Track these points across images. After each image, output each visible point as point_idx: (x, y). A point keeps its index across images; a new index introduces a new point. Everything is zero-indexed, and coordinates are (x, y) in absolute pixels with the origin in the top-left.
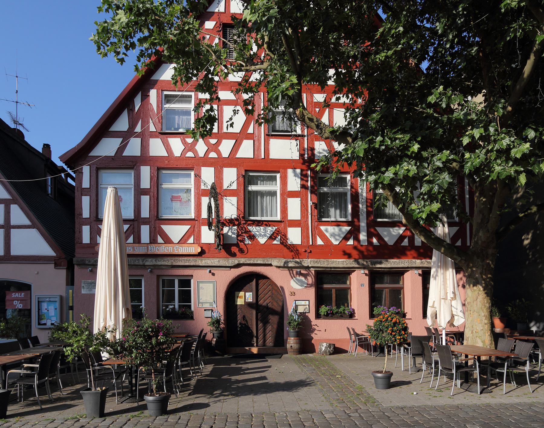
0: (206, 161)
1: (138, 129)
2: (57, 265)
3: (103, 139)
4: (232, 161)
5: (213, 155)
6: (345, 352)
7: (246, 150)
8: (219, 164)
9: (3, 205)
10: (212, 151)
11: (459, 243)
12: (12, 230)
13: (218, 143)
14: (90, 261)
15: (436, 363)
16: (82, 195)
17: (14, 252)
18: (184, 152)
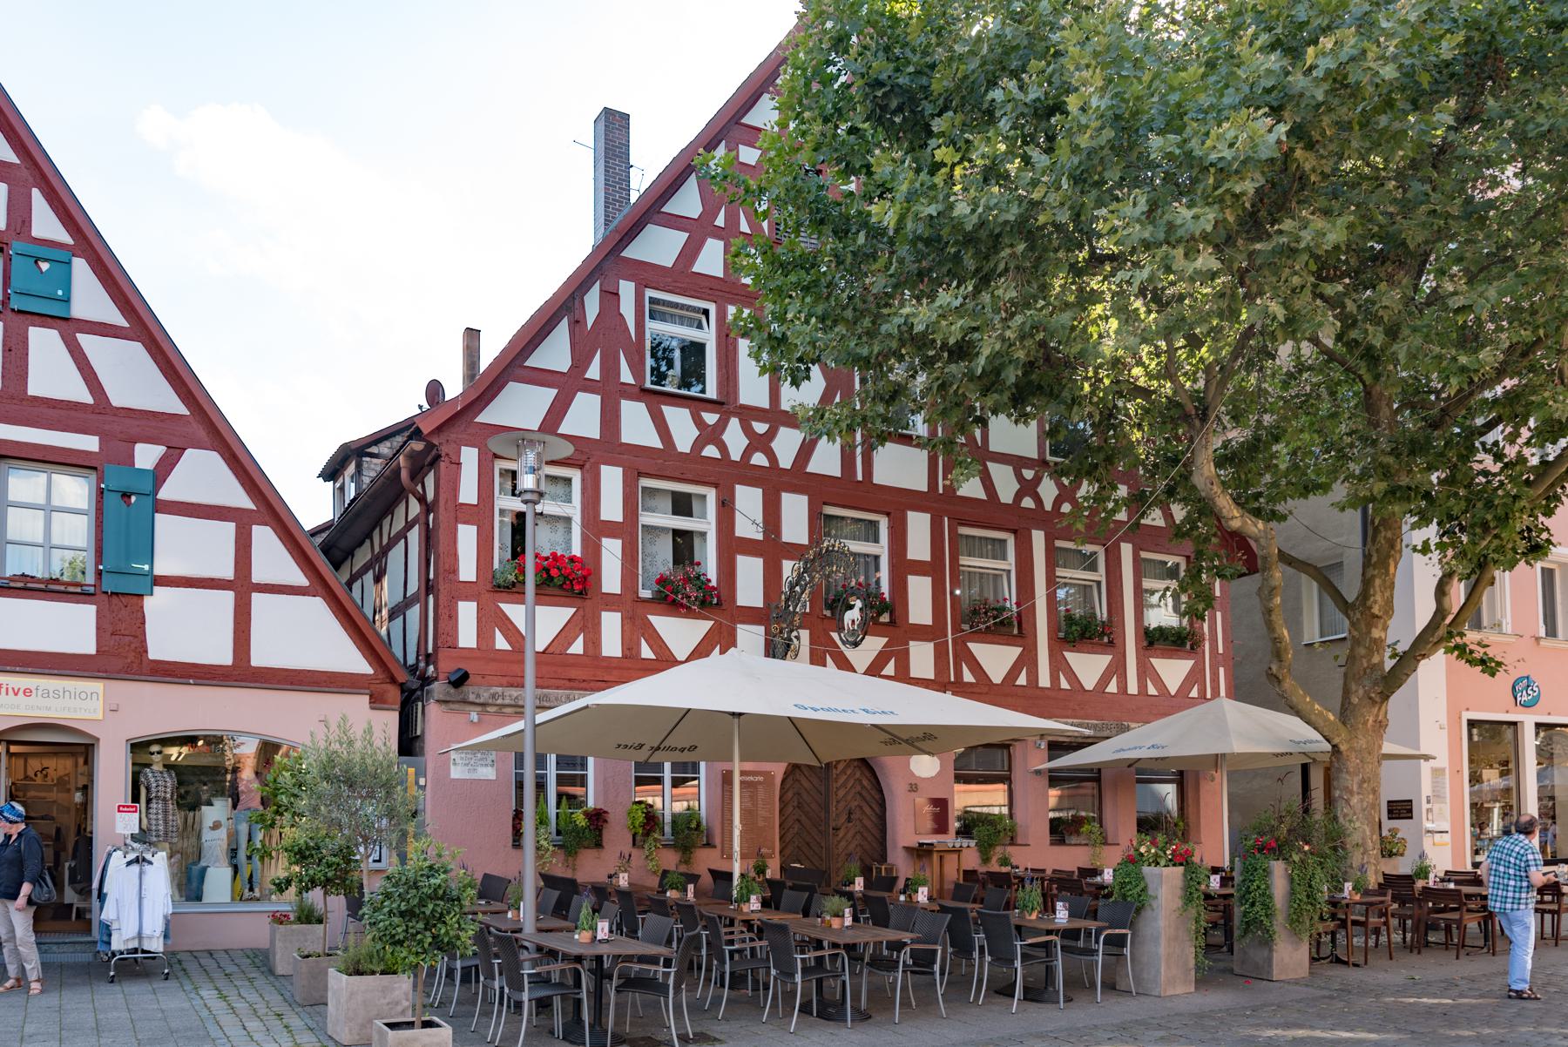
0: (744, 473)
1: (594, 372)
2: (377, 702)
3: (511, 384)
4: (799, 478)
5: (759, 459)
6: (387, 1025)
7: (827, 460)
8: (774, 483)
9: (233, 525)
10: (757, 450)
11: (1112, 687)
12: (255, 596)
13: (771, 434)
14: (478, 696)
15: (982, 948)
16: (457, 521)
17: (258, 660)
18: (698, 445)
